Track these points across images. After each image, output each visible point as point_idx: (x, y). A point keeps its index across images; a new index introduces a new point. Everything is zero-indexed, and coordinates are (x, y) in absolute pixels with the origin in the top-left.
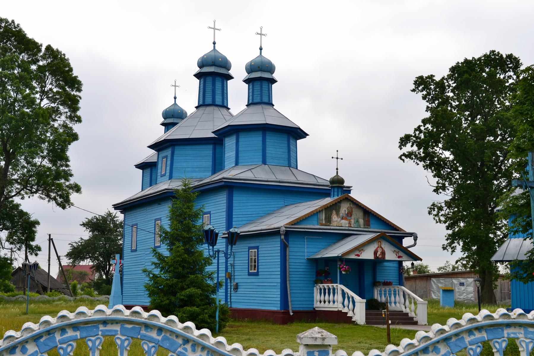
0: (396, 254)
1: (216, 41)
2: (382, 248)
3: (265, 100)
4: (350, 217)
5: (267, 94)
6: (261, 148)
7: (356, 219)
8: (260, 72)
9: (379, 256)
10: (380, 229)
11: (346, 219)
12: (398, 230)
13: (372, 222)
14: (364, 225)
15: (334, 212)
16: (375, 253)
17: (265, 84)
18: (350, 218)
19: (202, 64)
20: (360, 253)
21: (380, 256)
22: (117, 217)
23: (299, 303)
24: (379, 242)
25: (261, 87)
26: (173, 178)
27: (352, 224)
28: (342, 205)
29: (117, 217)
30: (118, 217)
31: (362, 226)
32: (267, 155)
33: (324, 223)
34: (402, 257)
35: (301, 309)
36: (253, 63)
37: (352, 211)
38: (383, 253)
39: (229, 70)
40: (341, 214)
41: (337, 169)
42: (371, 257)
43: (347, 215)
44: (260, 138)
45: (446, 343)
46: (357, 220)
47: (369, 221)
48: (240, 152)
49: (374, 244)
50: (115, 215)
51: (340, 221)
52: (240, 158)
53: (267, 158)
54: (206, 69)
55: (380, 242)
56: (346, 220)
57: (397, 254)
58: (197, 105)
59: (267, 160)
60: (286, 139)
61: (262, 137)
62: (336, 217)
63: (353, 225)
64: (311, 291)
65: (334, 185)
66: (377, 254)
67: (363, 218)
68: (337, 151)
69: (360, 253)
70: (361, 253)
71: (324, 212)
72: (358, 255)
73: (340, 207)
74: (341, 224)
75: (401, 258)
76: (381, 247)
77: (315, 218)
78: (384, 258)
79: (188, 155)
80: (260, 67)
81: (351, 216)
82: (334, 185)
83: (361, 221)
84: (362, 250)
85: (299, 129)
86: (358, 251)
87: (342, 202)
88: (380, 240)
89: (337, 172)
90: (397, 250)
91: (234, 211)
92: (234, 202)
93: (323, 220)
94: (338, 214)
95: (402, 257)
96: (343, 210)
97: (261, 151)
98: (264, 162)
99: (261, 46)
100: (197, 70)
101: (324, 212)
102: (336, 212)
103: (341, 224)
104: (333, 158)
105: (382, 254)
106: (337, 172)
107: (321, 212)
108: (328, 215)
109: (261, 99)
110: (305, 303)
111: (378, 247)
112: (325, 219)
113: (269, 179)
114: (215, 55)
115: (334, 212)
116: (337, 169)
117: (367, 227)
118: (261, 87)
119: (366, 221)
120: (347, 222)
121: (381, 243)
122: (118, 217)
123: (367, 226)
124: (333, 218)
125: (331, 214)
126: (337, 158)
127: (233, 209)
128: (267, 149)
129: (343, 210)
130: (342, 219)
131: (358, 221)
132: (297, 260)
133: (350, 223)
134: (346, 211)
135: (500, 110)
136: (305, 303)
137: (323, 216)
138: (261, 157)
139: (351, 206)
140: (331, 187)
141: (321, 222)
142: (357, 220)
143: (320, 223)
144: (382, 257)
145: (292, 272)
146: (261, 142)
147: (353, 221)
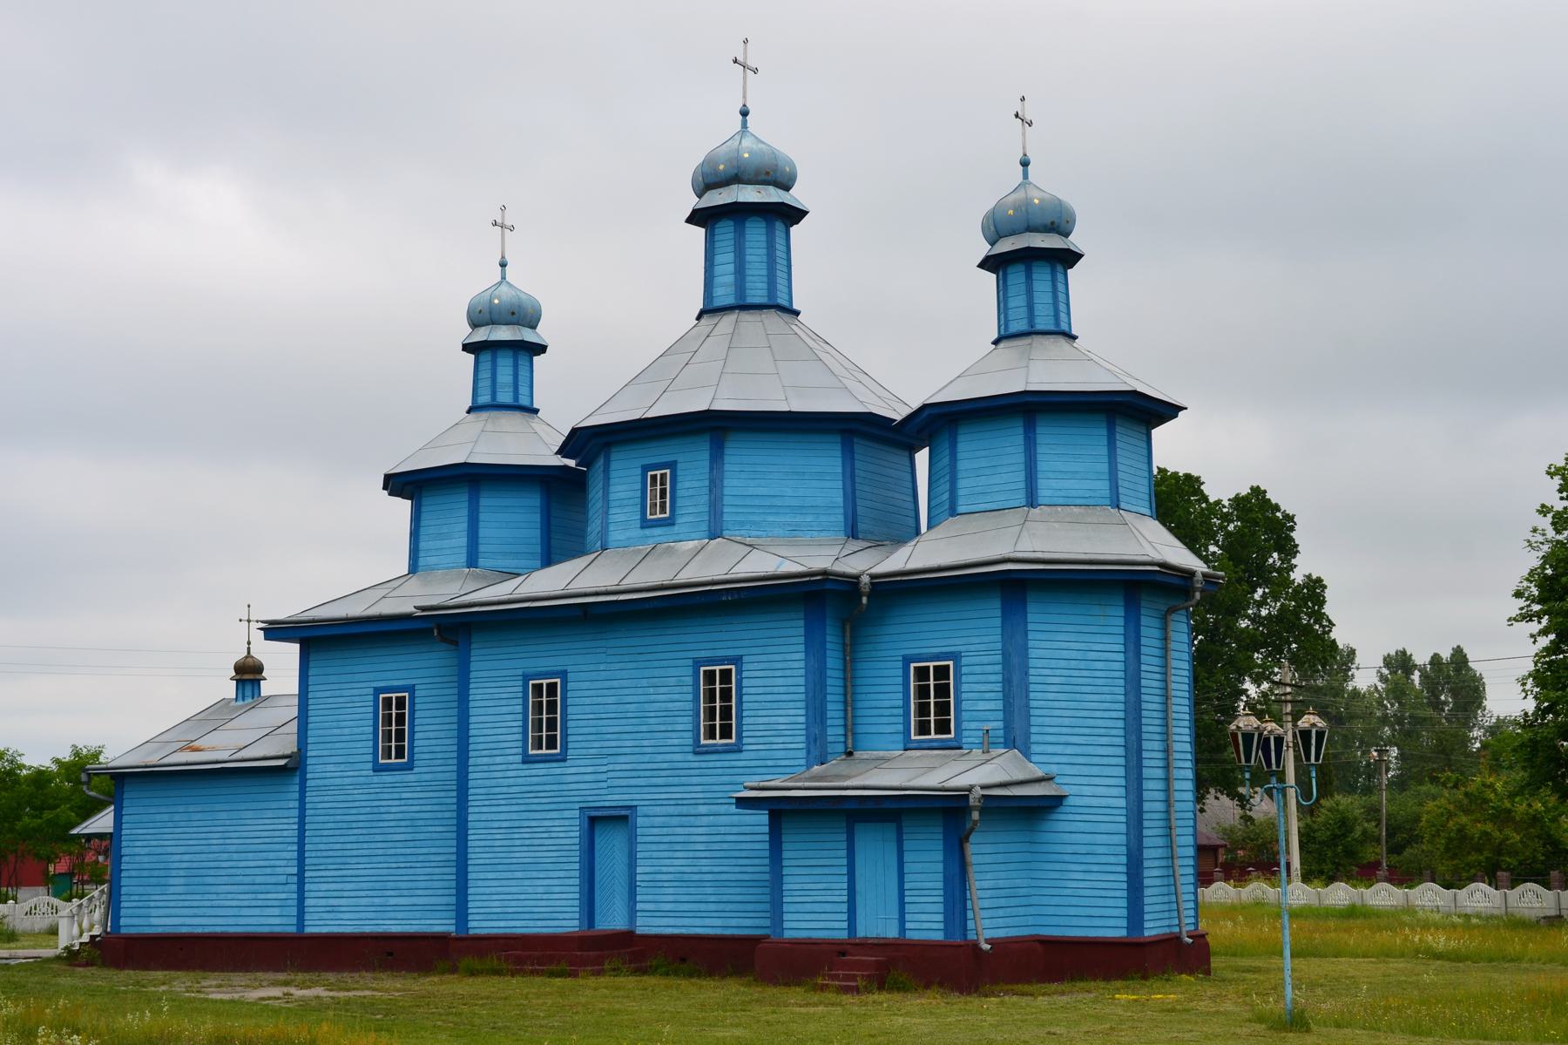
1: (508, 258)
17: (1042, 278)
19: (995, 229)
26: (420, 568)
39: (1067, 235)
41: (249, 643)
44: (464, 513)
45: (966, 940)
54: (1005, 246)
58: (995, 336)
65: (246, 677)
68: (249, 606)
80: (1056, 224)
82: (246, 677)
89: (249, 649)
99: (503, 257)
100: (983, 249)
104: (241, 620)
106: (249, 649)
114: (1027, 198)
116: (249, 643)
126: (249, 621)
138: (1022, 467)
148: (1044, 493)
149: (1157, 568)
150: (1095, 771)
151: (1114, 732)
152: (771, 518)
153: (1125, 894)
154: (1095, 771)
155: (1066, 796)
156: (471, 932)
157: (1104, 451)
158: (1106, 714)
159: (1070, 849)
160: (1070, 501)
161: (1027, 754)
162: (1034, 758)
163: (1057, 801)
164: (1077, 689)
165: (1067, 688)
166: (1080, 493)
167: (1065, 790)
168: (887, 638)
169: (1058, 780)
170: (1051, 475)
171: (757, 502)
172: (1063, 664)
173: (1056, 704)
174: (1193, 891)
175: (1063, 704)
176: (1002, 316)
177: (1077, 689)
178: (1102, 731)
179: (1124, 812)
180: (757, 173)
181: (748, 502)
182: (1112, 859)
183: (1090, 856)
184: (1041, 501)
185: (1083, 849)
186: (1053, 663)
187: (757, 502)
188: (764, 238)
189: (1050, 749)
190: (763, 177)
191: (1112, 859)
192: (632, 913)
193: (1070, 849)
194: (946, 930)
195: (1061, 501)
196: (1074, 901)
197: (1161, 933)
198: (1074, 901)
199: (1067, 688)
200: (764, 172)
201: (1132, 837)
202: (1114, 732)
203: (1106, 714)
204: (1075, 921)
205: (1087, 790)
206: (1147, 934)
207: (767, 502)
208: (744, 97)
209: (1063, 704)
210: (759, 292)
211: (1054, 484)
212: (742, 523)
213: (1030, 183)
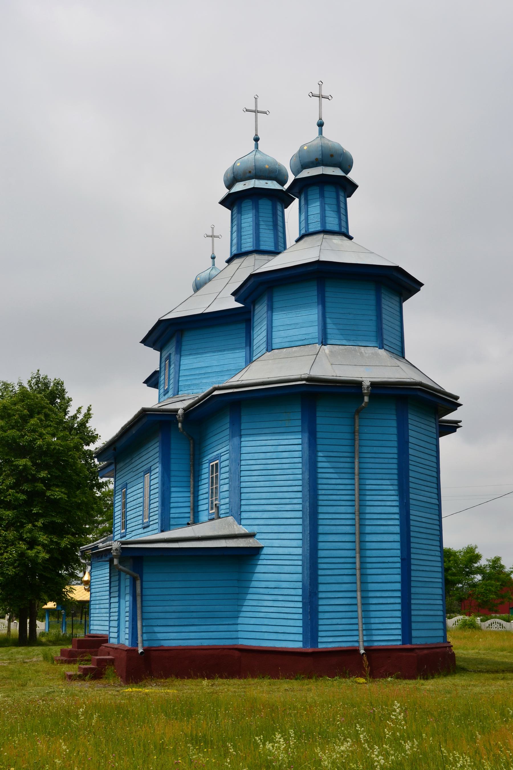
54: (239, 187)
148: (276, 341)
149: (304, 382)
150: (282, 529)
151: (295, 501)
152: (204, 381)
153: (301, 617)
154: (282, 529)
155: (262, 547)
156: (93, 632)
157: (373, 302)
158: (290, 489)
159: (264, 584)
160: (293, 344)
161: (239, 521)
162: (243, 522)
163: (256, 551)
164: (271, 472)
165: (264, 472)
166: (300, 337)
167: (261, 544)
168: (209, 447)
169: (258, 536)
170: (281, 328)
171: (197, 372)
172: (262, 456)
173: (258, 484)
174: (443, 621)
175: (262, 484)
176: (235, 235)
177: (271, 472)
178: (287, 501)
179: (300, 557)
180: (244, 173)
181: (193, 372)
182: (292, 592)
183: (277, 589)
184: (274, 347)
185: (272, 584)
186: (256, 456)
187: (197, 372)
188: (270, 207)
189: (253, 515)
190: (248, 175)
191: (292, 592)
192: (368, 630)
193: (264, 584)
194: (304, 641)
195: (287, 345)
196: (266, 621)
197: (350, 645)
198: (266, 621)
199: (264, 472)
200: (248, 172)
201: (306, 576)
202: (295, 501)
203: (290, 489)
204: (266, 636)
205: (276, 543)
206: (321, 646)
207: (203, 371)
208: (256, 130)
209: (262, 484)
210: (248, 245)
211: (282, 334)
212: (189, 386)
213: (324, 137)
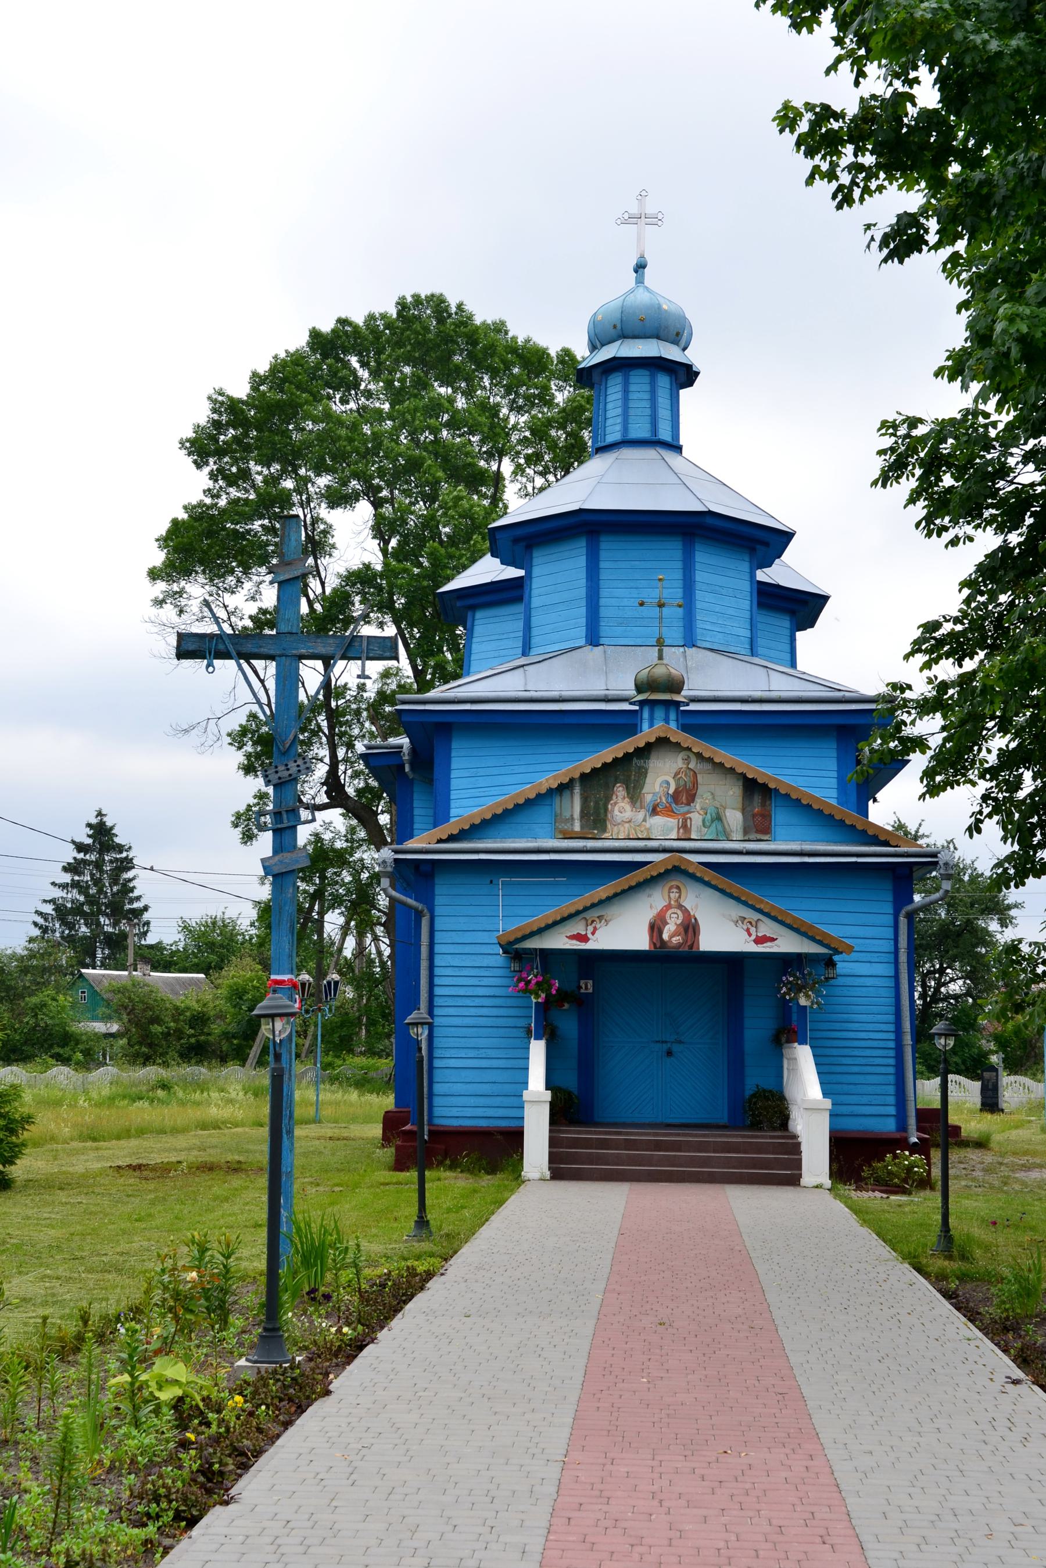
0: (748, 930)
2: (686, 911)
3: (665, 435)
4: (688, 804)
5: (648, 412)
6: (582, 592)
7: (711, 810)
8: (654, 342)
9: (671, 937)
10: (836, 842)
11: (669, 812)
12: (886, 844)
13: (780, 816)
14: (746, 831)
15: (620, 791)
16: (655, 928)
18: (686, 809)
20: (590, 929)
21: (676, 940)
22: (923, 836)
23: (472, 1101)
24: (671, 888)
25: (626, 392)
27: (694, 828)
28: (651, 765)
29: (923, 836)
30: (927, 836)
31: (738, 835)
32: (603, 612)
33: (577, 827)
34: (773, 940)
35: (483, 1123)
36: (600, 317)
37: (695, 784)
38: (690, 928)
40: (648, 798)
42: (639, 941)
43: (676, 797)
46: (718, 814)
47: (766, 817)
48: (533, 613)
49: (649, 896)
50: (917, 832)
51: (644, 820)
52: (535, 632)
53: (602, 624)
55: (678, 888)
56: (669, 816)
57: (753, 930)
59: (605, 630)
60: (678, 554)
61: (587, 555)
62: (628, 807)
63: (699, 831)
64: (520, 1063)
66: (661, 932)
67: (740, 806)
69: (590, 929)
70: (595, 929)
71: (577, 790)
72: (584, 938)
73: (643, 773)
74: (648, 830)
75: (769, 944)
76: (680, 907)
77: (543, 814)
78: (691, 947)
79: (505, 636)
81: (691, 798)
83: (734, 818)
84: (600, 918)
85: (711, 513)
86: (583, 922)
87: (654, 756)
88: (673, 883)
90: (752, 915)
91: (453, 804)
92: (453, 775)
93: (572, 818)
94: (634, 796)
95: (773, 940)
96: (659, 780)
97: (584, 603)
98: (593, 639)
101: (577, 790)
102: (627, 789)
103: (648, 830)
105: (686, 930)
107: (566, 794)
108: (597, 803)
109: (625, 429)
110: (498, 1101)
111: (669, 907)
112: (584, 815)
113: (566, 694)
115: (620, 791)
117: (759, 836)
118: (626, 392)
119: (754, 816)
120: (672, 822)
121: (680, 891)
122: (927, 836)
123: (758, 831)
124: (616, 812)
125: (608, 799)
127: (452, 797)
128: (603, 593)
129: (659, 780)
130: (654, 811)
131: (718, 818)
132: (464, 957)
133: (685, 826)
134: (668, 783)
135: (364, 364)
136: (498, 1101)
137: (574, 805)
139: (692, 766)
140: (642, 703)
141: (566, 827)
142: (718, 814)
143: (562, 832)
144: (685, 941)
145: (446, 999)
146: (582, 574)
147: (696, 819)
